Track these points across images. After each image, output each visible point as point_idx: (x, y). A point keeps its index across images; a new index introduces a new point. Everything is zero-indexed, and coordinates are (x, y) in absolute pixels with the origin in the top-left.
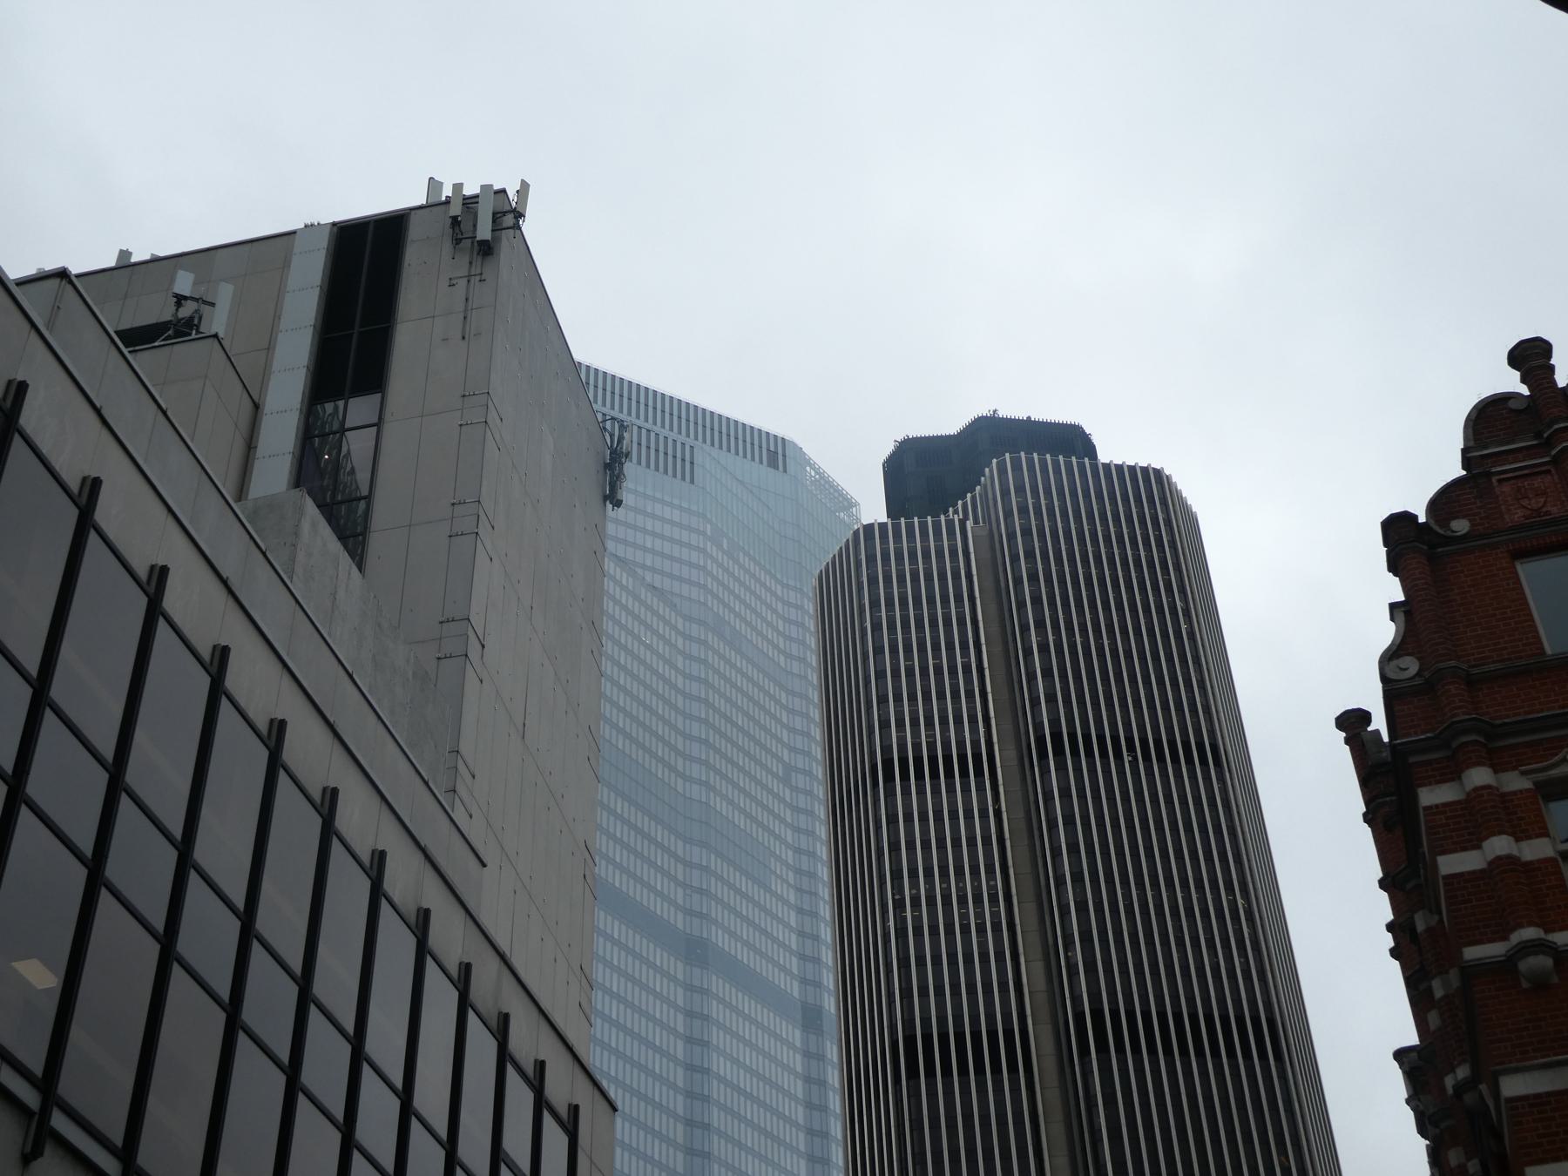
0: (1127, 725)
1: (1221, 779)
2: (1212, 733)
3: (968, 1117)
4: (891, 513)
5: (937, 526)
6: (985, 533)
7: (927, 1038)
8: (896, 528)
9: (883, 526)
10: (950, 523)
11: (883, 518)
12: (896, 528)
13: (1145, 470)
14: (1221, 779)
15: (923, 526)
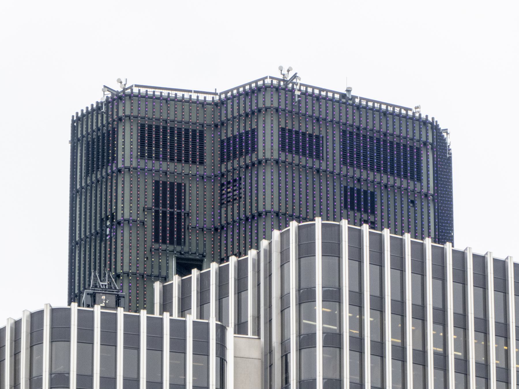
4: (74, 296)
5: (132, 326)
8: (86, 321)
9: (60, 316)
10: (155, 326)
12: (86, 321)
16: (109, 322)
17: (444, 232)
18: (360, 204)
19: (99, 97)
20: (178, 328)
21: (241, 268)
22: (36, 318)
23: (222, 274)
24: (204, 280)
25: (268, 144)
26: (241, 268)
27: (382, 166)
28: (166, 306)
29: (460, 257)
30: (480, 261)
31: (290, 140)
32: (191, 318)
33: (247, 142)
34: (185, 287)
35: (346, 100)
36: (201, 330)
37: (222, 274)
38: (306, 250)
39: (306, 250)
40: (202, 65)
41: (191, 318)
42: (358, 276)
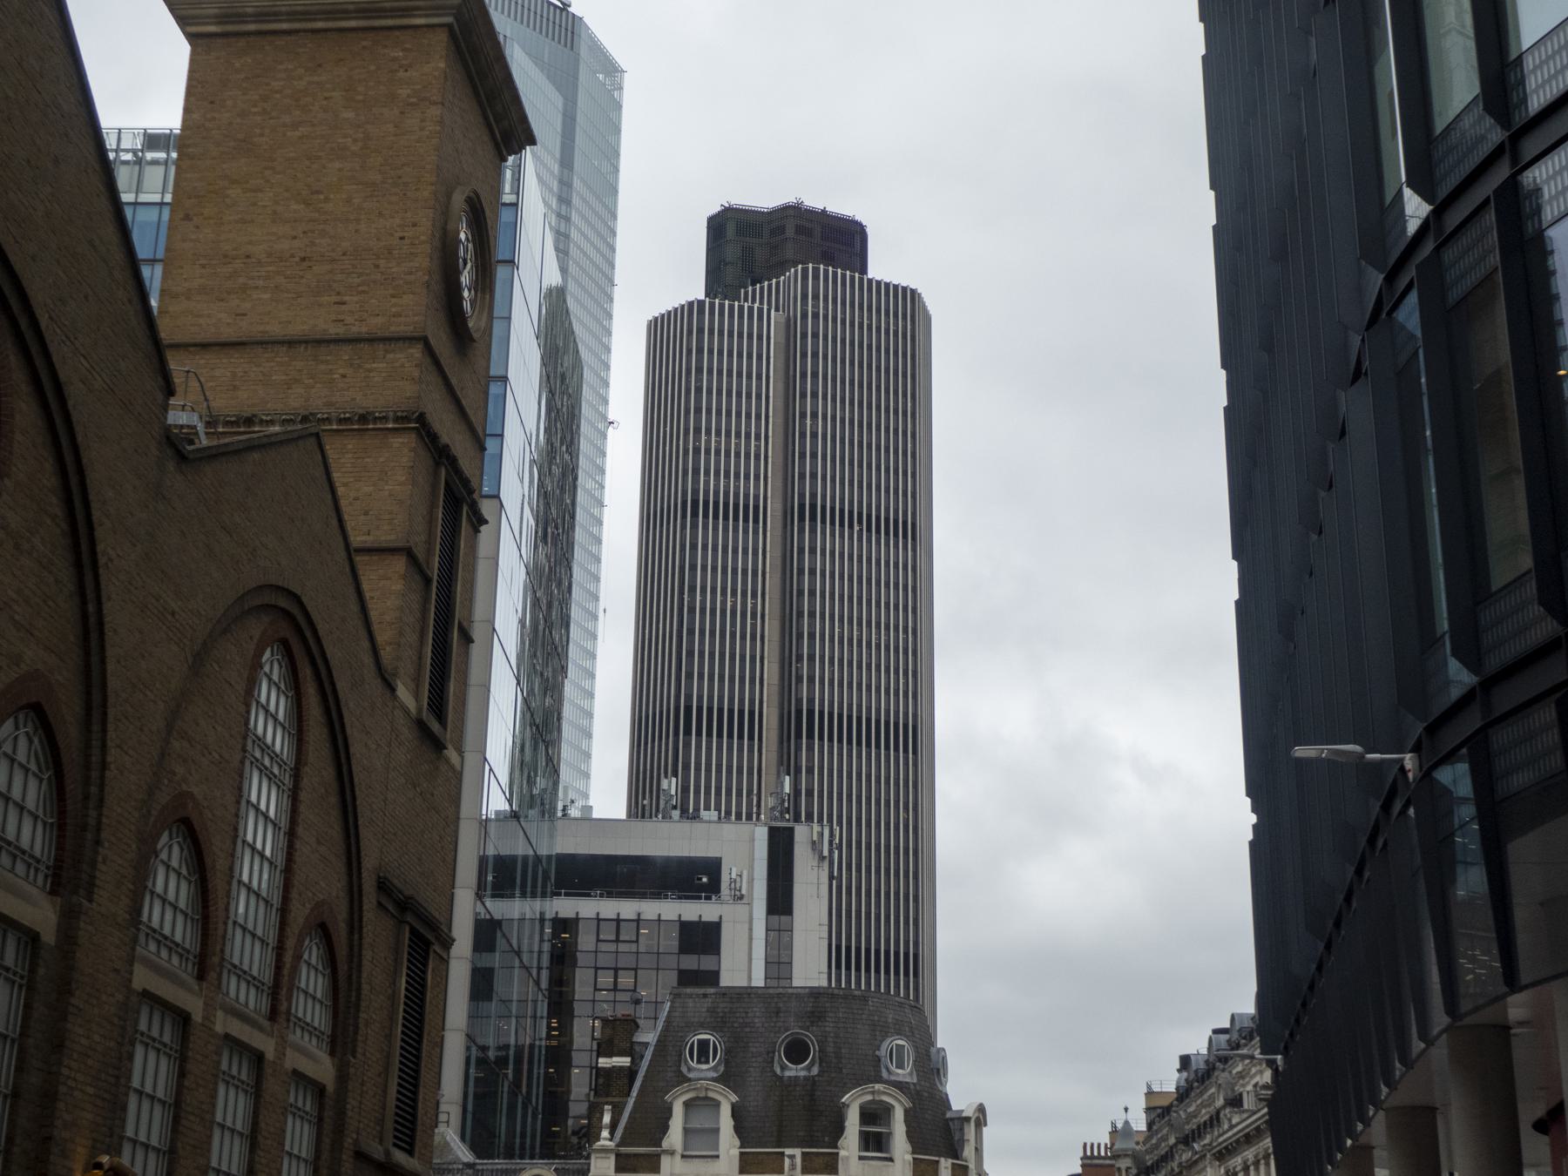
0: (905, 548)
1: (914, 550)
2: (914, 514)
3: (719, 766)
4: (707, 295)
5: (731, 308)
6: (783, 321)
7: (700, 709)
8: (712, 306)
9: (701, 303)
10: (741, 308)
11: (702, 296)
12: (712, 306)
13: (905, 289)
14: (914, 550)
15: (722, 306)
16: (722, 306)
17: (864, 270)
18: (829, 259)
19: (719, 209)
20: (751, 309)
21: (778, 284)
22: (691, 304)
23: (770, 286)
24: (762, 289)
25: (790, 232)
26: (778, 284)
27: (840, 240)
28: (746, 300)
29: (870, 281)
30: (879, 283)
31: (800, 230)
32: (756, 305)
33: (782, 229)
34: (754, 291)
35: (824, 211)
36: (760, 310)
37: (770, 286)
38: (805, 277)
39: (805, 277)
40: (764, 198)
41: (756, 305)
42: (159, 993)
